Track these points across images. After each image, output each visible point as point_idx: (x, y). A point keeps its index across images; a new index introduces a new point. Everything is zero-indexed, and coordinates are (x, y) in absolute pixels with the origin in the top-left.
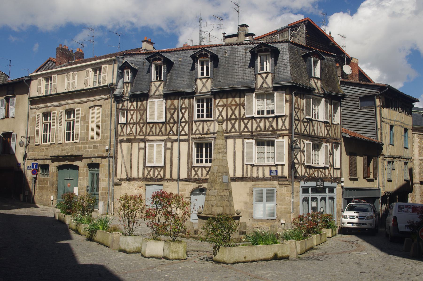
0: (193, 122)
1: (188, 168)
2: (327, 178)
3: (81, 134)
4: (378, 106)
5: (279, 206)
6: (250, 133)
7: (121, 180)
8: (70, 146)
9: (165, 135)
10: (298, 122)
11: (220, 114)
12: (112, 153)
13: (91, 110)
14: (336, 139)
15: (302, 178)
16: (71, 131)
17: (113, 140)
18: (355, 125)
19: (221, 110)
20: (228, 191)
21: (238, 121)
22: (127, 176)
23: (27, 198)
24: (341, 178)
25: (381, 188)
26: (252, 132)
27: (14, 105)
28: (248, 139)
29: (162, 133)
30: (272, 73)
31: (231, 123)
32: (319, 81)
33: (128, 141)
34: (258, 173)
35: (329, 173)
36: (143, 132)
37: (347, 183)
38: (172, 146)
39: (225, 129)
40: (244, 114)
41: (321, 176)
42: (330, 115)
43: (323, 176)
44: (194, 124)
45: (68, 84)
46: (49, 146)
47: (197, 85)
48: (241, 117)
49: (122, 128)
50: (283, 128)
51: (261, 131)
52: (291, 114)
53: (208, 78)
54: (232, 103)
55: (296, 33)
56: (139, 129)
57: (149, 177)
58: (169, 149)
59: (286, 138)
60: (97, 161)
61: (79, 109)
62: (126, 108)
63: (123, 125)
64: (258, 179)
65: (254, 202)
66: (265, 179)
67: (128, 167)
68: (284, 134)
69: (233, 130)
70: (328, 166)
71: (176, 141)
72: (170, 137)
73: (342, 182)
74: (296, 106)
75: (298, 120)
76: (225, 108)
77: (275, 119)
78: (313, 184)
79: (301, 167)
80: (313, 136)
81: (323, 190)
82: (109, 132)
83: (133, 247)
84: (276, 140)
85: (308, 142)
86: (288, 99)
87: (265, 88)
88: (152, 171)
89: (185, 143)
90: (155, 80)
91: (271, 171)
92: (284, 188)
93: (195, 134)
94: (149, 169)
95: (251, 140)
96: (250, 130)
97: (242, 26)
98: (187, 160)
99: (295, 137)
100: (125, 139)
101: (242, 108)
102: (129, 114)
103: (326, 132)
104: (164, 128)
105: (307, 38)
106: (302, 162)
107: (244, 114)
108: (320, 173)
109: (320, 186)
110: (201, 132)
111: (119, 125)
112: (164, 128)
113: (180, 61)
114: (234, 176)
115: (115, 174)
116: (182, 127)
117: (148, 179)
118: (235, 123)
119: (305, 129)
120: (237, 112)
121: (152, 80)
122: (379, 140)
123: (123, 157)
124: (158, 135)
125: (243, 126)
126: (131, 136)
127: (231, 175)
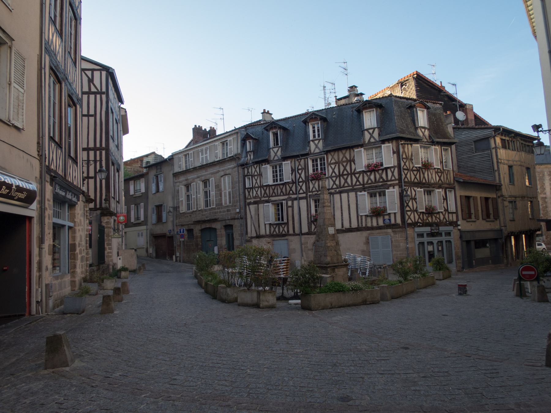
0: (310, 181)
1: (308, 223)
2: (442, 223)
3: (216, 200)
4: (493, 148)
5: (394, 253)
6: (362, 186)
7: (252, 238)
8: (209, 212)
9: (286, 195)
10: (407, 171)
11: (333, 171)
12: (243, 214)
13: (222, 179)
14: (449, 184)
15: (414, 225)
16: (209, 199)
17: (242, 203)
18: (471, 168)
19: (333, 168)
20: (334, 241)
21: (350, 176)
22: (256, 233)
23: (178, 258)
24: (457, 222)
25: (503, 228)
26: (363, 185)
27: (163, 181)
28: (361, 192)
29: (283, 193)
30: (378, 128)
31: (344, 178)
32: (427, 130)
33: (255, 203)
34: (372, 222)
35: (444, 218)
36: (267, 194)
37: (463, 225)
38: (293, 204)
39: (339, 185)
40: (355, 169)
41: (436, 221)
42: (440, 162)
43: (437, 220)
44: (310, 182)
45: (202, 158)
46: (191, 213)
47: (310, 147)
48: (353, 172)
49: (249, 192)
50: (393, 178)
51: (372, 183)
52: (399, 164)
53: (319, 140)
54: (343, 160)
55: (406, 87)
56: (263, 192)
57: (275, 233)
58: (290, 207)
59: (397, 188)
60: (231, 223)
61: (213, 179)
62: (251, 174)
63: (249, 190)
64: (372, 228)
65: (371, 250)
66: (379, 228)
67: (257, 226)
68: (394, 184)
69: (346, 185)
70: (443, 211)
71: (296, 199)
72: (290, 196)
73: (459, 225)
74: (404, 156)
75: (407, 170)
76: (337, 165)
77: (385, 170)
78: (428, 229)
79: (414, 214)
80: (424, 183)
81: (439, 234)
82: (238, 196)
83: (232, 297)
84: (387, 191)
85: (419, 189)
86: (395, 150)
87: (373, 142)
88: (277, 227)
89: (304, 200)
90: (273, 146)
91: (384, 220)
92: (398, 235)
93: (312, 192)
94: (275, 226)
95: (363, 193)
96: (362, 183)
97: (351, 87)
98: (306, 215)
99: (405, 186)
100: (252, 201)
101: (352, 163)
102: (254, 179)
103: (438, 178)
104: (284, 188)
105: (417, 91)
106: (415, 208)
107: (355, 169)
108: (434, 218)
109: (435, 231)
110: (318, 189)
111: (246, 190)
112: (284, 188)
113: (294, 127)
114: (350, 226)
115: (247, 233)
116: (300, 186)
117: (275, 235)
118: (347, 178)
119: (415, 178)
120: (348, 168)
121: (271, 147)
122: (498, 182)
123: (251, 217)
124: (280, 195)
125: (354, 180)
126: (257, 198)
127: (339, 226)
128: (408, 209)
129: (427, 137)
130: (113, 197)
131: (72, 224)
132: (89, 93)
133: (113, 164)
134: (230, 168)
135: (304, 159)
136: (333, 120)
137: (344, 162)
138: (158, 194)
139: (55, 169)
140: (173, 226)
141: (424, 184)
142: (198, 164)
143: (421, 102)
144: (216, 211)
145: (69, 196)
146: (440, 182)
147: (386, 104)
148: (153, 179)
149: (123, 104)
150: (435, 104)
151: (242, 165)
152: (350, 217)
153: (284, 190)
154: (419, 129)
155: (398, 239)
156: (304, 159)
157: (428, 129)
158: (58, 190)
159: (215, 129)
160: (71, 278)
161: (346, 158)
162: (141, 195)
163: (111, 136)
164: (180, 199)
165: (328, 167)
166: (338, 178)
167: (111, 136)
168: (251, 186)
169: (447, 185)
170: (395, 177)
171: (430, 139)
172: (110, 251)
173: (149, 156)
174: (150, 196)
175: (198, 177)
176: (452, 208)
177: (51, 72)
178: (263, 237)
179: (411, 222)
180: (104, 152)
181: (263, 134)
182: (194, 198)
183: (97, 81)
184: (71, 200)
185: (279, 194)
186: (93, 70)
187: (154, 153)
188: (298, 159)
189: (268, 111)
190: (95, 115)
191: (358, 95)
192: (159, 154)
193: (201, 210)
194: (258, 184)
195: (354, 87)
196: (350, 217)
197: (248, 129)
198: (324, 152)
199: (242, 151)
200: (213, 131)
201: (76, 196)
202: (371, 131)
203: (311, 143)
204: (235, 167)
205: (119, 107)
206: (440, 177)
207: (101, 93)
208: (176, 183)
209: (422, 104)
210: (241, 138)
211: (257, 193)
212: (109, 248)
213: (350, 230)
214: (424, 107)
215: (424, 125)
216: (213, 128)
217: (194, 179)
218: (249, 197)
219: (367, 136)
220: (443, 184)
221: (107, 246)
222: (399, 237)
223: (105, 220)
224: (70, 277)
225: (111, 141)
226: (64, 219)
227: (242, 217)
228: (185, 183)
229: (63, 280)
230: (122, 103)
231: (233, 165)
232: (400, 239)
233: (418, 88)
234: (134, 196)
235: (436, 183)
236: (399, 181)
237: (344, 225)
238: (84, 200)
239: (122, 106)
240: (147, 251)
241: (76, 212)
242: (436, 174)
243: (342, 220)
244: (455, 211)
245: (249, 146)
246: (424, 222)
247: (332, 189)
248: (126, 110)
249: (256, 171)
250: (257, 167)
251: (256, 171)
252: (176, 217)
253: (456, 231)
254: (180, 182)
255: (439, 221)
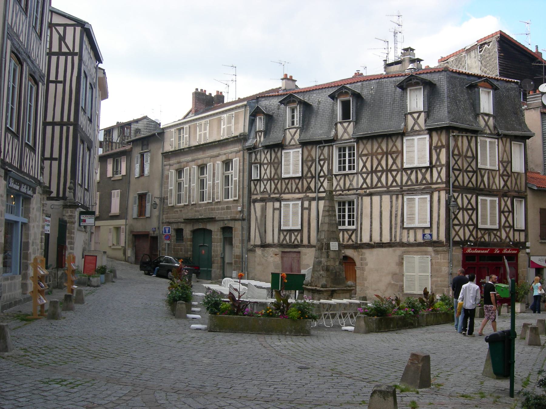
0: (333, 176)
6: (399, 188)
7: (255, 246)
11: (364, 166)
12: (246, 214)
21: (385, 173)
24: (525, 243)
26: (388, 187)
27: (149, 162)
29: (299, 190)
30: (425, 112)
31: (377, 176)
32: (491, 118)
33: (262, 200)
35: (508, 236)
36: (278, 190)
38: (310, 205)
45: (200, 135)
48: (389, 168)
49: (255, 186)
50: (439, 181)
54: (378, 152)
56: (273, 186)
57: (285, 242)
58: (306, 209)
60: (231, 224)
63: (256, 182)
68: (440, 188)
71: (314, 199)
72: (308, 194)
73: (528, 248)
75: (459, 170)
79: (464, 230)
88: (288, 235)
91: (424, 235)
97: (406, 50)
99: (454, 191)
100: (259, 198)
103: (502, 183)
104: (300, 183)
108: (493, 237)
110: (343, 188)
111: (252, 182)
112: (300, 183)
114: (381, 240)
119: (470, 181)
121: (287, 127)
124: (295, 193)
125: (390, 179)
128: (456, 222)
129: (492, 128)
130: (79, 184)
131: (25, 220)
132: (60, 53)
133: (83, 142)
134: (234, 152)
135: (328, 146)
136: (370, 96)
137: (379, 154)
138: (142, 178)
139: (10, 161)
140: (159, 223)
141: (482, 190)
142: (194, 143)
143: (486, 81)
144: (213, 207)
145: (24, 189)
146: (506, 188)
147: (438, 80)
148: (138, 159)
149: (102, 63)
150: (509, 84)
151: (249, 149)
152: (381, 228)
153: (300, 186)
154: (480, 116)
155: (439, 261)
156: (328, 146)
157: (494, 117)
158: (12, 185)
159: (223, 94)
160: (22, 280)
161: (382, 149)
162: (121, 178)
163: (82, 107)
164: (170, 188)
165: (358, 160)
166: (370, 175)
167: (82, 107)
168: (259, 178)
169: (515, 193)
170: (441, 179)
171: (495, 130)
172: (72, 251)
173: (140, 122)
174: (133, 180)
175: (193, 161)
176: (520, 224)
177: (13, 55)
178: (269, 246)
179: (459, 240)
180: (71, 128)
181: (279, 109)
182: (187, 187)
183: (69, 39)
184: (26, 194)
185: (293, 191)
186: (65, 26)
187: (145, 118)
188: (321, 145)
189: (291, 77)
190: (64, 82)
191: (413, 61)
192: (153, 119)
193: (194, 204)
194: (267, 176)
195: (409, 50)
196: (381, 228)
197: (260, 101)
198: (354, 138)
199: (250, 130)
200: (220, 98)
201: (31, 189)
202: (416, 115)
203: (339, 125)
204: (239, 151)
205: (97, 68)
206: (506, 182)
207: (73, 54)
208: (165, 165)
209: (487, 82)
210: (250, 112)
211: (265, 188)
212: (71, 247)
213: (381, 245)
214: (491, 87)
215: (489, 110)
216: (221, 93)
217: (188, 162)
218: (255, 193)
219: (410, 121)
220: (509, 192)
221: (69, 244)
222: (441, 258)
223: (68, 212)
224: (21, 279)
225: (81, 113)
226: (17, 215)
227: (244, 217)
228: (177, 166)
229: (13, 281)
230: (101, 62)
231: (237, 147)
232: (442, 261)
233: (502, 54)
234: (112, 179)
235: (500, 189)
236: (446, 184)
237: (373, 238)
238: (41, 192)
239: (100, 66)
240: (125, 253)
241: (31, 206)
242: (501, 177)
243: (371, 231)
244: (523, 228)
245: (260, 124)
246: (478, 240)
247: (361, 188)
248: (105, 71)
249: (266, 157)
250: (267, 153)
251: (266, 157)
252: (163, 212)
253: (524, 255)
254: (170, 165)
255: (499, 240)
